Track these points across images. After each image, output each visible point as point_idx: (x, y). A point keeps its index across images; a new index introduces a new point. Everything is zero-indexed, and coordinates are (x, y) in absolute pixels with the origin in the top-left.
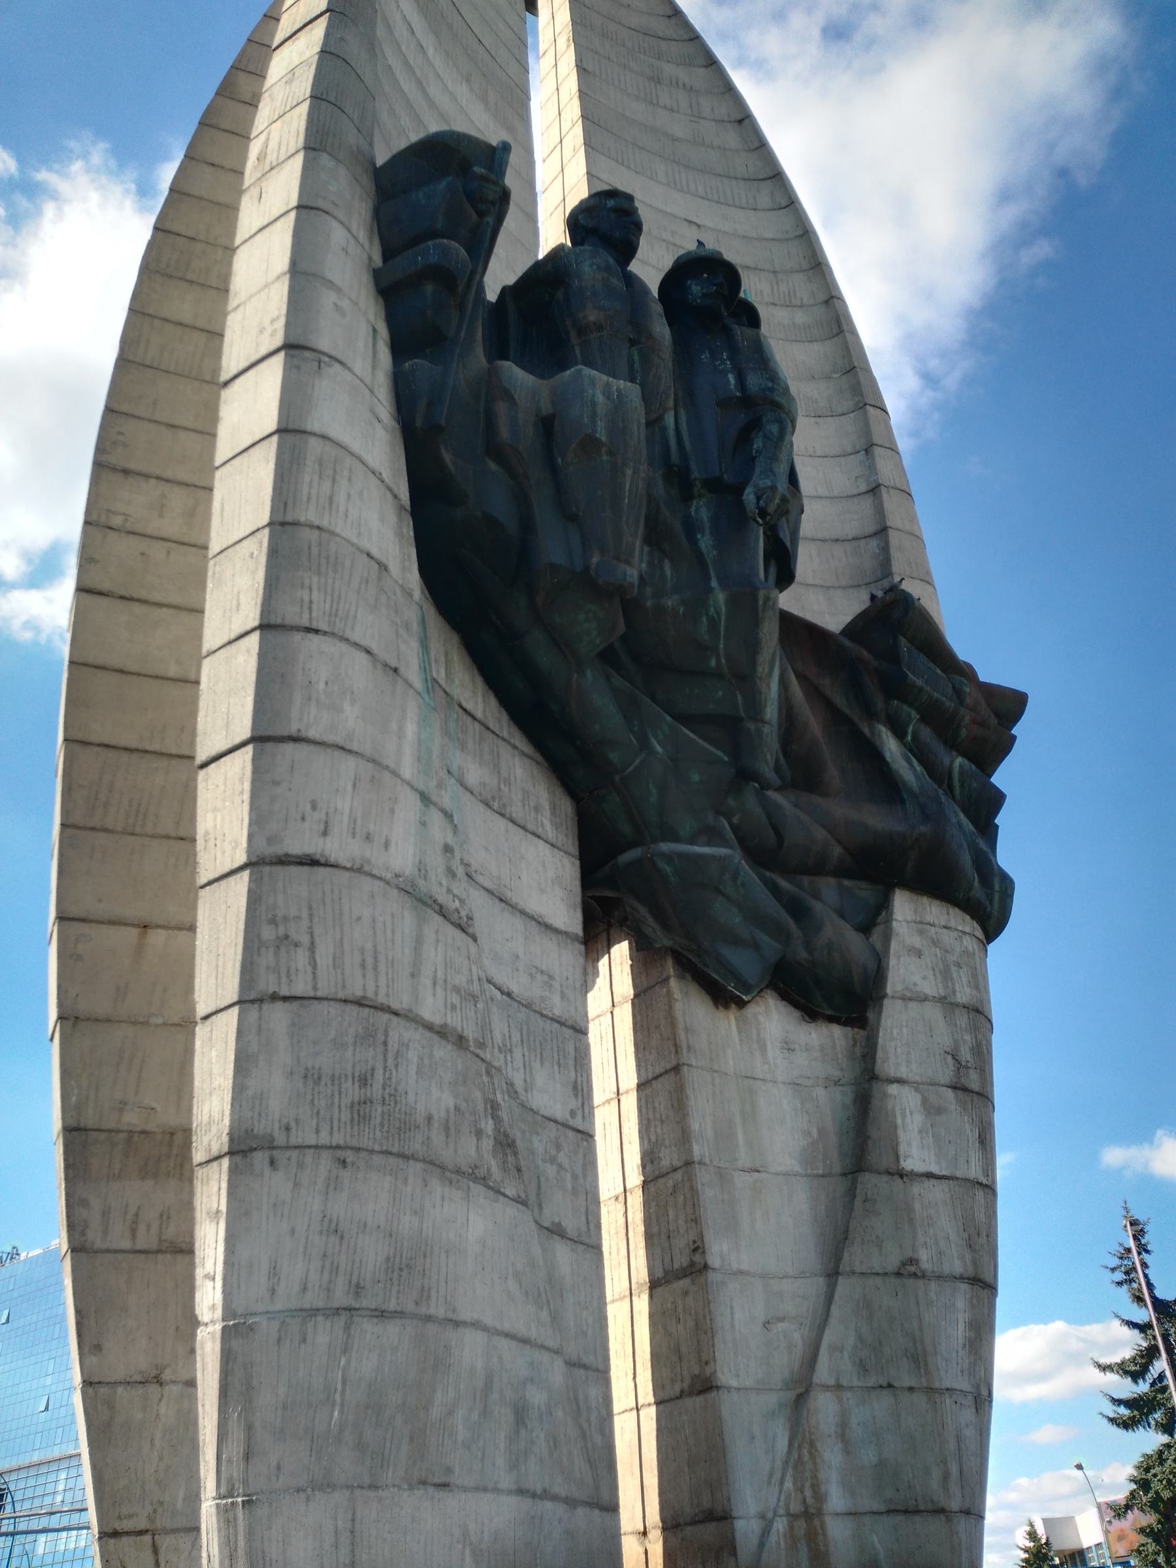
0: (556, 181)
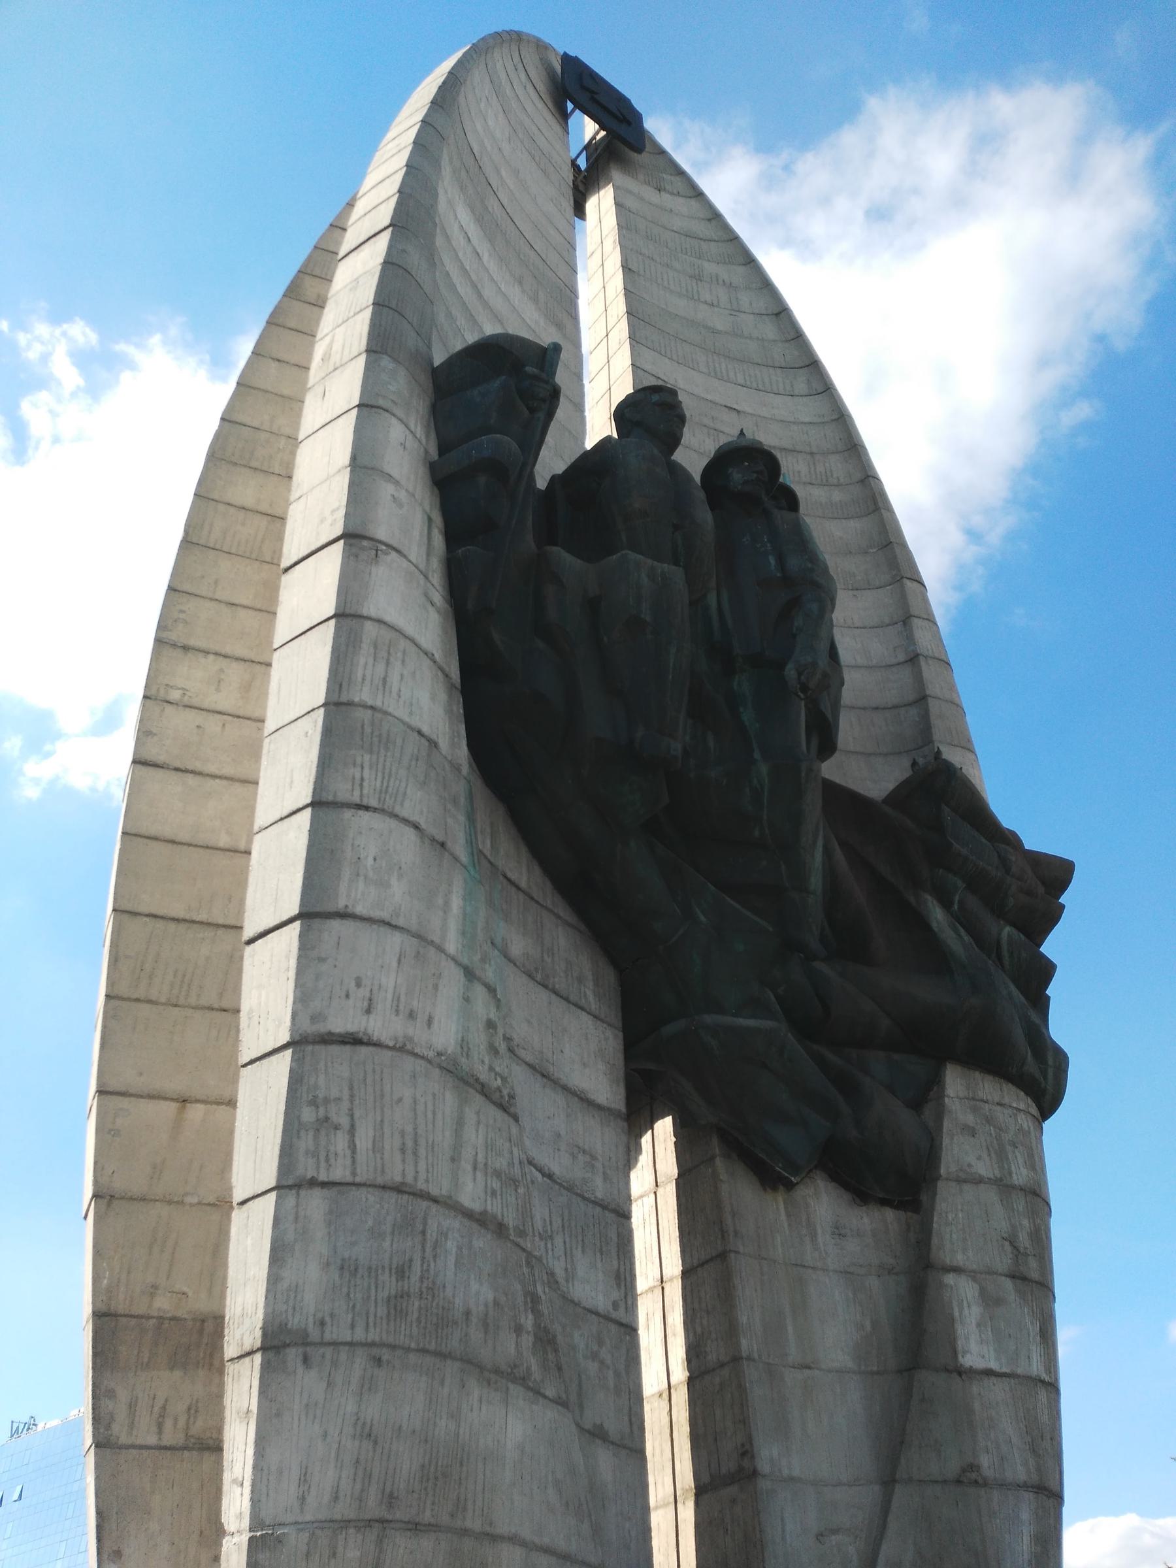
0: (602, 381)
